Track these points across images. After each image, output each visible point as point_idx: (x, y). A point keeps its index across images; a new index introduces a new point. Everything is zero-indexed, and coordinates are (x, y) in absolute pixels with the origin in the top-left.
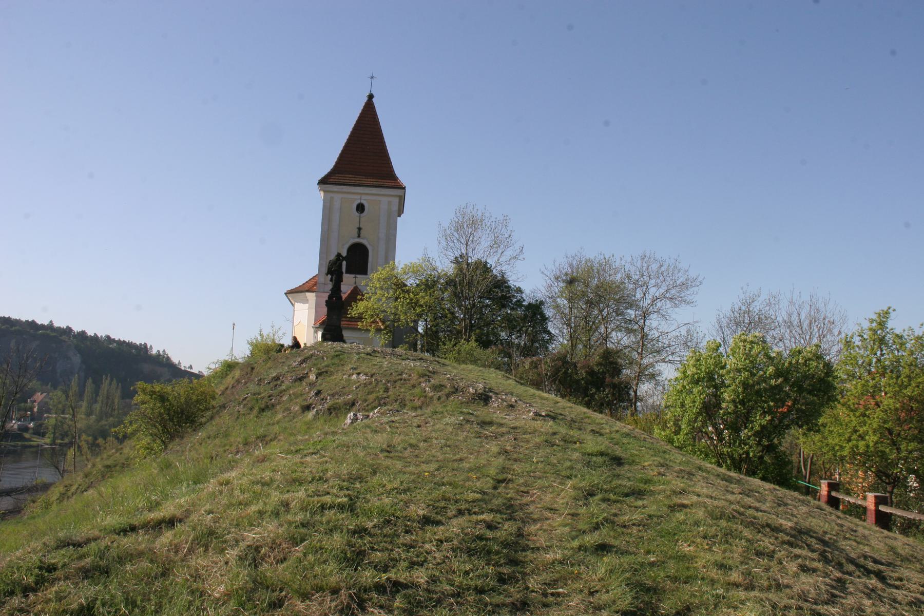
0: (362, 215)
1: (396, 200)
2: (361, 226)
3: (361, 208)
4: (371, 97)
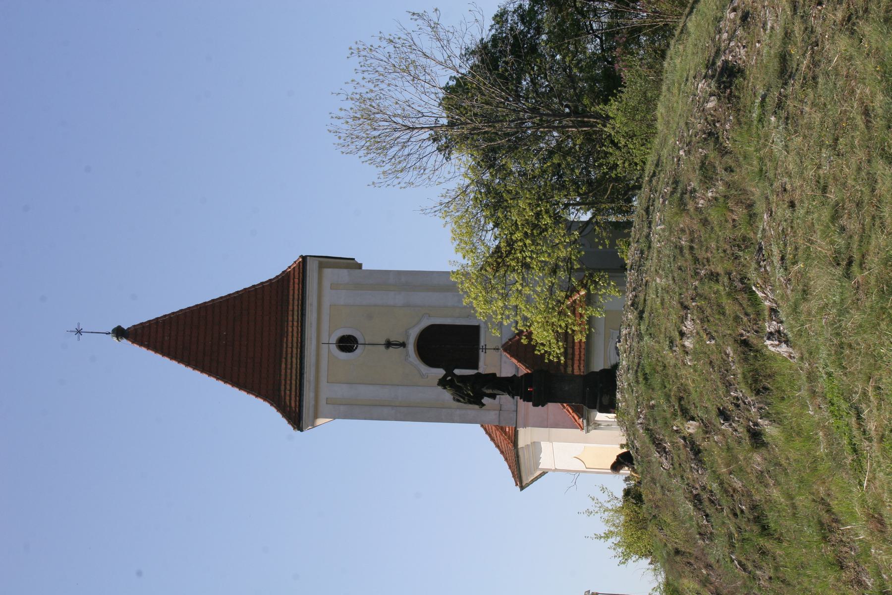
0: (360, 341)
1: (329, 274)
2: (383, 342)
3: (347, 344)
4: (119, 333)
